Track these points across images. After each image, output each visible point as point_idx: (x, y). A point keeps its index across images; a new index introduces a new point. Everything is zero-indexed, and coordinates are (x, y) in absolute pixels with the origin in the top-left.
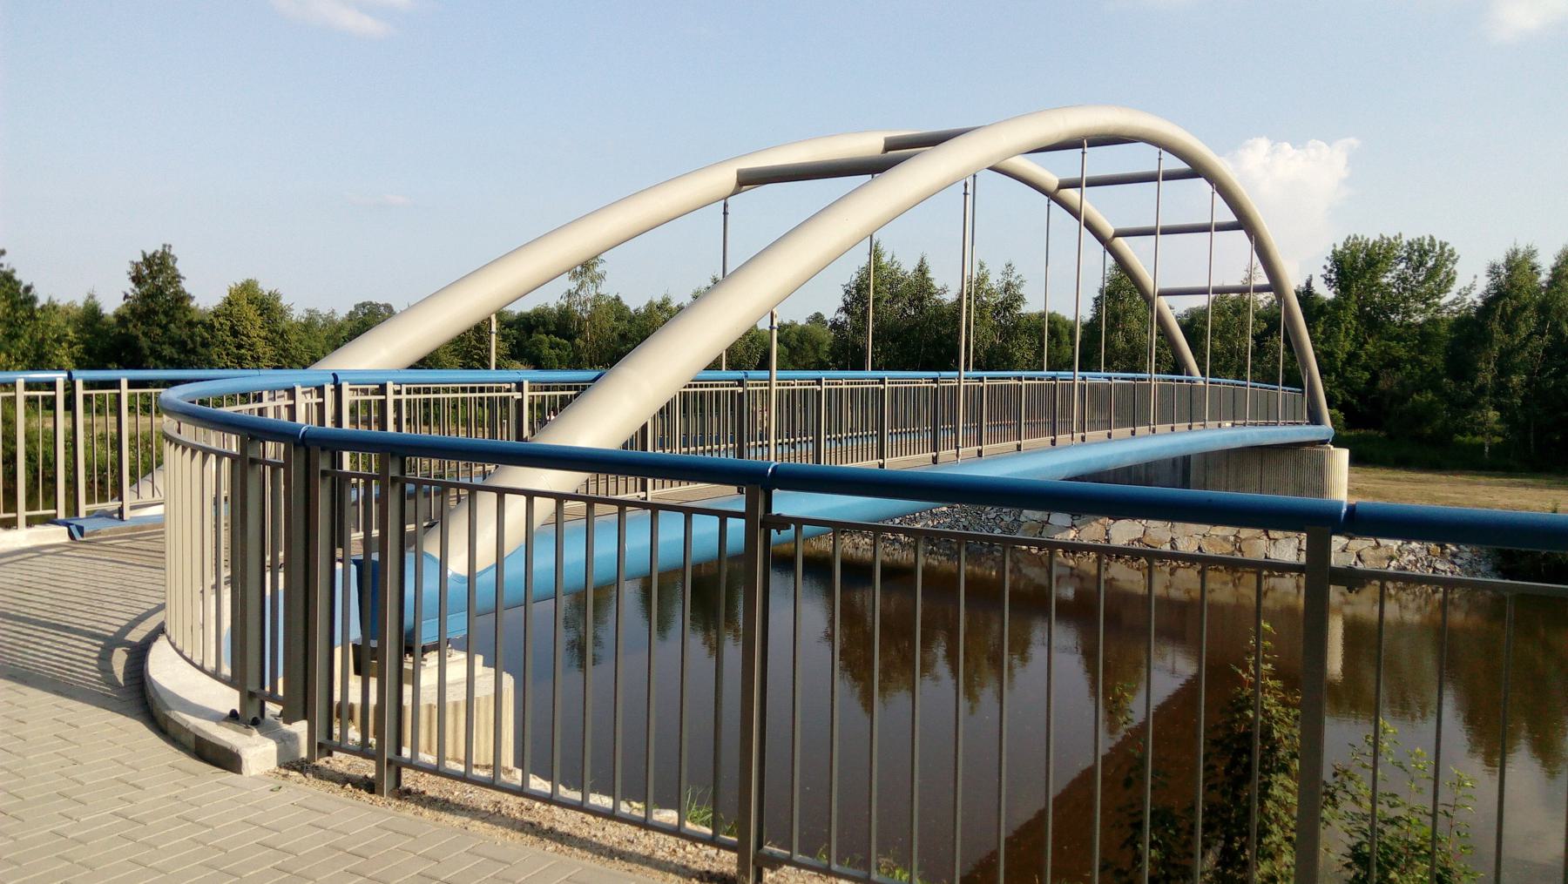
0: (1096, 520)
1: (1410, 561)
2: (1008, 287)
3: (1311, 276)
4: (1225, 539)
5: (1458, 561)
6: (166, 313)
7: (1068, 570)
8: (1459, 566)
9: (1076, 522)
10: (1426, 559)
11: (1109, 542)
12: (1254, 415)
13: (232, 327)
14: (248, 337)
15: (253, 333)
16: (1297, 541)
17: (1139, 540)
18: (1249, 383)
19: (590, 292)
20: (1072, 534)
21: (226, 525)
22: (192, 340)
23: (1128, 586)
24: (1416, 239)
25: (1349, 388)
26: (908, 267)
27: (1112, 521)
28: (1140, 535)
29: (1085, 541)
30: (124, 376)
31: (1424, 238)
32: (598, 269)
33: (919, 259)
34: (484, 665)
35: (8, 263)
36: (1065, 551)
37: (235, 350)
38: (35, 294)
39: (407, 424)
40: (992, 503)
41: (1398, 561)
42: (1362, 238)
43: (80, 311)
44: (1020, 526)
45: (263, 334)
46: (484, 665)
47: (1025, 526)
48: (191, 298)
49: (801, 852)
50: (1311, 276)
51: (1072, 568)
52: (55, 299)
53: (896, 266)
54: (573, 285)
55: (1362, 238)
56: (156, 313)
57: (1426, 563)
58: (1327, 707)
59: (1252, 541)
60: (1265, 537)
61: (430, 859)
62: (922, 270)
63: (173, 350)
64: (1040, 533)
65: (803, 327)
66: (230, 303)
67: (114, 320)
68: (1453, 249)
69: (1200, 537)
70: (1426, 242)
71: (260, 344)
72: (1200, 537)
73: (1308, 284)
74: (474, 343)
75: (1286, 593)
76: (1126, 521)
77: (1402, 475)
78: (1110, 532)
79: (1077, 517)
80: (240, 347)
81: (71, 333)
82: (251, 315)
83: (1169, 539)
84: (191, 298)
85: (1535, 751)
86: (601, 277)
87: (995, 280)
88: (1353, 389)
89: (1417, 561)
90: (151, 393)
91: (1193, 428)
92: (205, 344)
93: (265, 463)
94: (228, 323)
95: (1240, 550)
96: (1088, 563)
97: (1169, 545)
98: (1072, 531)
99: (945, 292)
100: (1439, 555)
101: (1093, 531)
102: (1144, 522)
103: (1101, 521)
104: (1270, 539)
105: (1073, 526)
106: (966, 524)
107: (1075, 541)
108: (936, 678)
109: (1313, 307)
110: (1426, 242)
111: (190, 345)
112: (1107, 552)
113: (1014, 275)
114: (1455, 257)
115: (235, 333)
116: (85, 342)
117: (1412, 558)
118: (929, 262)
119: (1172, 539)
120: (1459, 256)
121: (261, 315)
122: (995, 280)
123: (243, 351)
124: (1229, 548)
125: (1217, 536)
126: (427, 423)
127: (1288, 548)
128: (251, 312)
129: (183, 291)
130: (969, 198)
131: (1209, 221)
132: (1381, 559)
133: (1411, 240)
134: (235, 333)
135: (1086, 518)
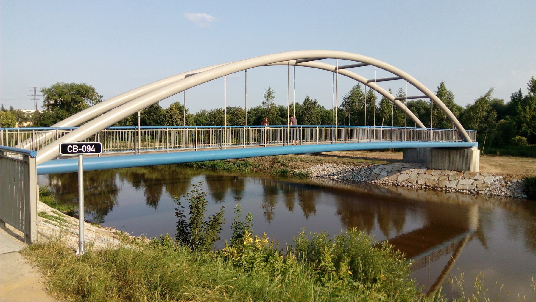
1: (493, 188)
3: (521, 89)
5: (510, 188)
6: (154, 113)
7: (386, 190)
8: (510, 190)
9: (389, 174)
10: (499, 187)
12: (339, 138)
13: (171, 116)
14: (175, 119)
15: (177, 118)
16: (457, 181)
18: (432, 129)
19: (270, 102)
22: (159, 120)
30: (443, 129)
32: (272, 95)
37: (171, 123)
41: (489, 188)
44: (371, 175)
45: (180, 118)
47: (373, 175)
50: (521, 89)
51: (387, 189)
52: (280, 105)
54: (265, 100)
56: (151, 112)
57: (499, 189)
63: (154, 123)
65: (327, 112)
66: (170, 109)
68: (530, 81)
69: (427, 179)
71: (179, 121)
72: (427, 179)
73: (520, 91)
74: (235, 119)
75: (454, 199)
77: (525, 159)
80: (173, 122)
81: (129, 119)
82: (176, 112)
83: (416, 180)
85: (134, 185)
86: (273, 97)
89: (496, 188)
91: (333, 143)
92: (163, 121)
94: (170, 115)
95: (438, 184)
97: (415, 182)
100: (504, 186)
106: (355, 174)
111: (159, 122)
113: (403, 92)
115: (172, 118)
116: (133, 121)
117: (495, 187)
119: (417, 180)
121: (179, 112)
123: (174, 123)
124: (435, 183)
126: (200, 144)
128: (176, 112)
129: (159, 106)
130: (36, 107)
131: (374, 79)
132: (484, 187)
134: (172, 118)
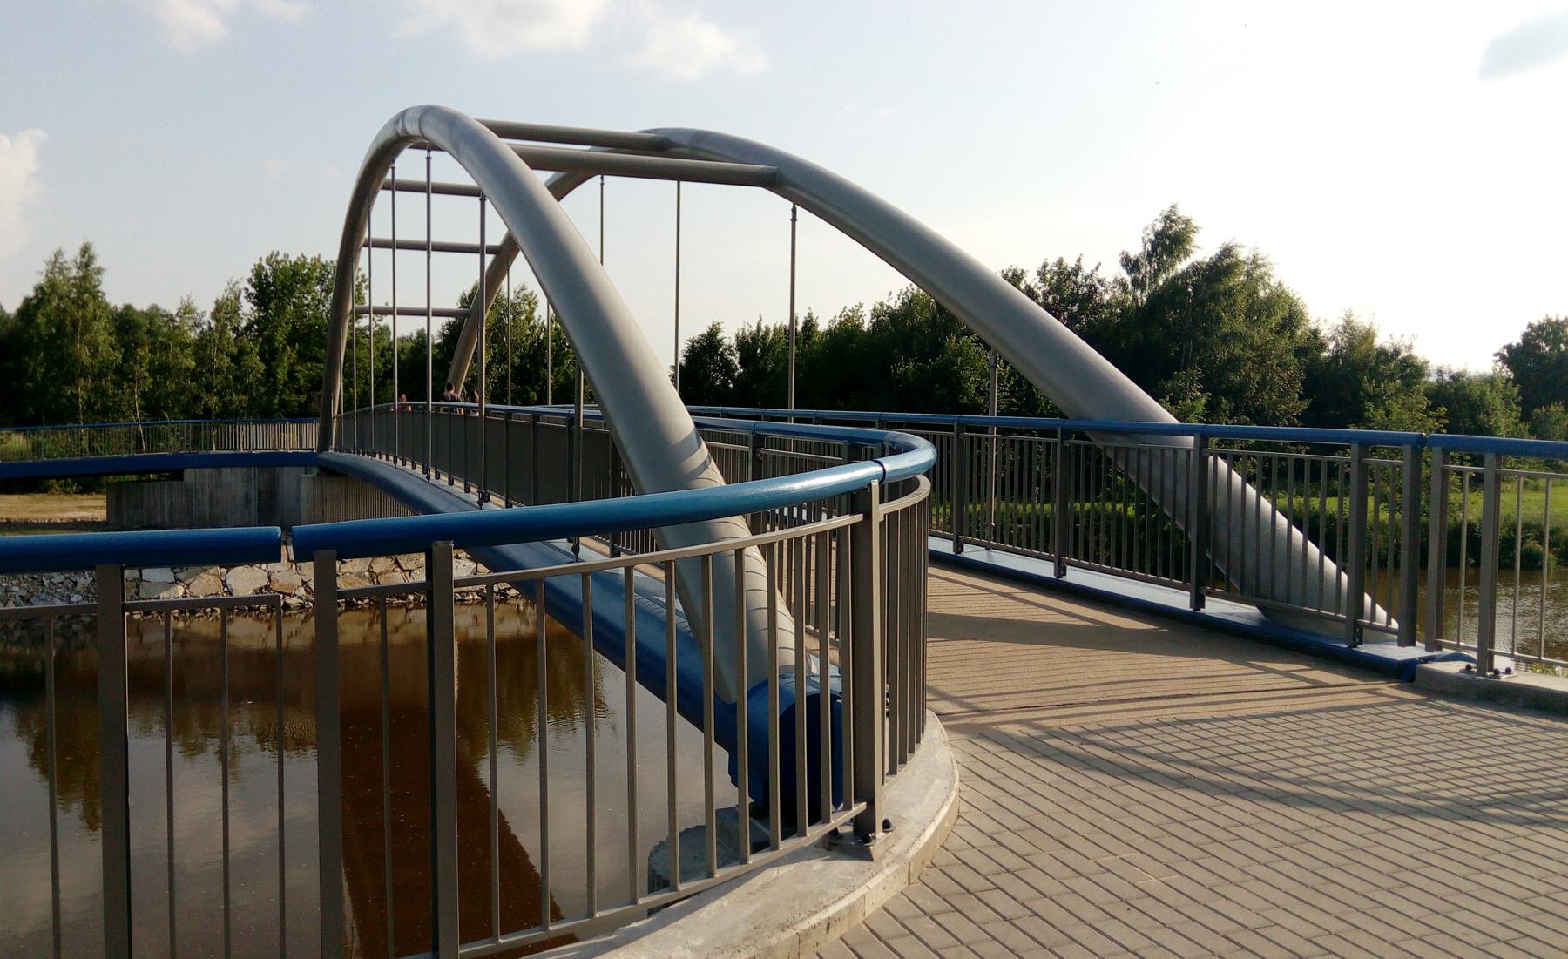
0: (206, 571)
4: (360, 575)
9: (180, 576)
11: (231, 594)
17: (267, 587)
20: (180, 590)
23: (256, 645)
27: (224, 570)
28: (265, 582)
29: (202, 597)
35: (2, 304)
36: (181, 612)
38: (1194, 239)
39: (1426, 527)
40: (60, 569)
43: (9, 325)
49: (1545, 656)
58: (1263, 617)
59: (388, 575)
60: (398, 569)
64: (138, 594)
67: (1506, 372)
76: (242, 567)
78: (228, 582)
90: (829, 517)
93: (1459, 641)
96: (205, 626)
98: (179, 587)
101: (205, 583)
102: (264, 566)
103: (212, 571)
104: (404, 571)
105: (177, 581)
107: (189, 598)
108: (766, 327)
112: (232, 606)
125: (351, 573)
127: (414, 568)
135: (192, 570)
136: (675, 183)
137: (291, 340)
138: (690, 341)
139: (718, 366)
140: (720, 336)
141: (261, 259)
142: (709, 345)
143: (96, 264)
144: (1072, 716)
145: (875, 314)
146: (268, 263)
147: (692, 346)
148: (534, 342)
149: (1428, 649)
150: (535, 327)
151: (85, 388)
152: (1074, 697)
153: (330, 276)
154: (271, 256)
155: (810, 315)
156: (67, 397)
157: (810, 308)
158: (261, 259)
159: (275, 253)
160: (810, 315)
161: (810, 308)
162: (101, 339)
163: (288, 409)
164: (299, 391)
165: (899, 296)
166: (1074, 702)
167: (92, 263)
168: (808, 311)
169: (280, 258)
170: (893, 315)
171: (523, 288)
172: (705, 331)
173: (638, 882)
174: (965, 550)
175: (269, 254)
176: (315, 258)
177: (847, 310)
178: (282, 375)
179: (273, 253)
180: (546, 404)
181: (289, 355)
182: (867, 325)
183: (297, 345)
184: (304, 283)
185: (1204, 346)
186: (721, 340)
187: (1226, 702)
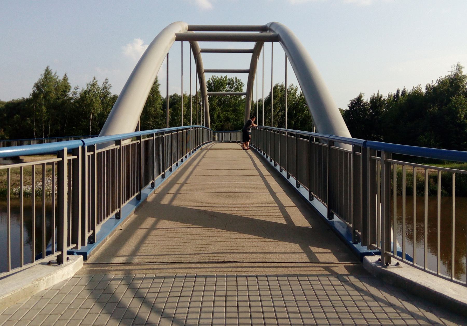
2: (104, 88)
21: (56, 171)
24: (231, 78)
25: (216, 128)
26: (61, 77)
31: (233, 78)
33: (64, 74)
34: (67, 255)
42: (218, 77)
46: (67, 255)
48: (171, 95)
53: (56, 77)
55: (218, 77)
61: (132, 319)
62: (65, 79)
70: (234, 79)
79: (454, 74)
84: (171, 95)
87: (100, 84)
88: (217, 128)
99: (77, 89)
109: (385, 101)
110: (234, 79)
114: (243, 85)
118: (68, 76)
120: (244, 84)
122: (100, 84)
133: (229, 78)
136: (181, 42)
137: (219, 105)
138: (351, 101)
139: (353, 109)
140: (362, 99)
141: (209, 78)
142: (358, 102)
143: (158, 83)
144: (208, 268)
145: (427, 88)
146: (211, 80)
147: (352, 103)
148: (295, 104)
149: (368, 249)
150: (296, 98)
151: (153, 122)
152: (166, 260)
153: (231, 83)
154: (212, 77)
155: (404, 89)
156: (147, 124)
157: (404, 87)
158: (209, 78)
159: (213, 76)
160: (404, 89)
161: (404, 87)
162: (158, 106)
163: (218, 128)
164: (221, 122)
165: (437, 81)
166: (183, 261)
167: (157, 82)
168: (404, 88)
169: (215, 78)
170: (434, 88)
171: (292, 85)
172: (357, 96)
173: (324, 315)
174: (300, 187)
175: (211, 77)
176: (225, 76)
177: (415, 88)
178: (216, 115)
179: (212, 76)
180: (182, 126)
181: (218, 109)
182: (424, 91)
183: (221, 106)
184: (223, 85)
185: (97, 98)
186: (362, 100)
187: (298, 267)
